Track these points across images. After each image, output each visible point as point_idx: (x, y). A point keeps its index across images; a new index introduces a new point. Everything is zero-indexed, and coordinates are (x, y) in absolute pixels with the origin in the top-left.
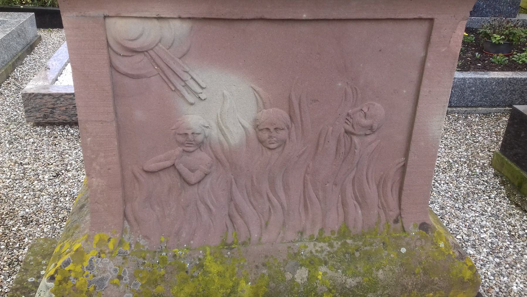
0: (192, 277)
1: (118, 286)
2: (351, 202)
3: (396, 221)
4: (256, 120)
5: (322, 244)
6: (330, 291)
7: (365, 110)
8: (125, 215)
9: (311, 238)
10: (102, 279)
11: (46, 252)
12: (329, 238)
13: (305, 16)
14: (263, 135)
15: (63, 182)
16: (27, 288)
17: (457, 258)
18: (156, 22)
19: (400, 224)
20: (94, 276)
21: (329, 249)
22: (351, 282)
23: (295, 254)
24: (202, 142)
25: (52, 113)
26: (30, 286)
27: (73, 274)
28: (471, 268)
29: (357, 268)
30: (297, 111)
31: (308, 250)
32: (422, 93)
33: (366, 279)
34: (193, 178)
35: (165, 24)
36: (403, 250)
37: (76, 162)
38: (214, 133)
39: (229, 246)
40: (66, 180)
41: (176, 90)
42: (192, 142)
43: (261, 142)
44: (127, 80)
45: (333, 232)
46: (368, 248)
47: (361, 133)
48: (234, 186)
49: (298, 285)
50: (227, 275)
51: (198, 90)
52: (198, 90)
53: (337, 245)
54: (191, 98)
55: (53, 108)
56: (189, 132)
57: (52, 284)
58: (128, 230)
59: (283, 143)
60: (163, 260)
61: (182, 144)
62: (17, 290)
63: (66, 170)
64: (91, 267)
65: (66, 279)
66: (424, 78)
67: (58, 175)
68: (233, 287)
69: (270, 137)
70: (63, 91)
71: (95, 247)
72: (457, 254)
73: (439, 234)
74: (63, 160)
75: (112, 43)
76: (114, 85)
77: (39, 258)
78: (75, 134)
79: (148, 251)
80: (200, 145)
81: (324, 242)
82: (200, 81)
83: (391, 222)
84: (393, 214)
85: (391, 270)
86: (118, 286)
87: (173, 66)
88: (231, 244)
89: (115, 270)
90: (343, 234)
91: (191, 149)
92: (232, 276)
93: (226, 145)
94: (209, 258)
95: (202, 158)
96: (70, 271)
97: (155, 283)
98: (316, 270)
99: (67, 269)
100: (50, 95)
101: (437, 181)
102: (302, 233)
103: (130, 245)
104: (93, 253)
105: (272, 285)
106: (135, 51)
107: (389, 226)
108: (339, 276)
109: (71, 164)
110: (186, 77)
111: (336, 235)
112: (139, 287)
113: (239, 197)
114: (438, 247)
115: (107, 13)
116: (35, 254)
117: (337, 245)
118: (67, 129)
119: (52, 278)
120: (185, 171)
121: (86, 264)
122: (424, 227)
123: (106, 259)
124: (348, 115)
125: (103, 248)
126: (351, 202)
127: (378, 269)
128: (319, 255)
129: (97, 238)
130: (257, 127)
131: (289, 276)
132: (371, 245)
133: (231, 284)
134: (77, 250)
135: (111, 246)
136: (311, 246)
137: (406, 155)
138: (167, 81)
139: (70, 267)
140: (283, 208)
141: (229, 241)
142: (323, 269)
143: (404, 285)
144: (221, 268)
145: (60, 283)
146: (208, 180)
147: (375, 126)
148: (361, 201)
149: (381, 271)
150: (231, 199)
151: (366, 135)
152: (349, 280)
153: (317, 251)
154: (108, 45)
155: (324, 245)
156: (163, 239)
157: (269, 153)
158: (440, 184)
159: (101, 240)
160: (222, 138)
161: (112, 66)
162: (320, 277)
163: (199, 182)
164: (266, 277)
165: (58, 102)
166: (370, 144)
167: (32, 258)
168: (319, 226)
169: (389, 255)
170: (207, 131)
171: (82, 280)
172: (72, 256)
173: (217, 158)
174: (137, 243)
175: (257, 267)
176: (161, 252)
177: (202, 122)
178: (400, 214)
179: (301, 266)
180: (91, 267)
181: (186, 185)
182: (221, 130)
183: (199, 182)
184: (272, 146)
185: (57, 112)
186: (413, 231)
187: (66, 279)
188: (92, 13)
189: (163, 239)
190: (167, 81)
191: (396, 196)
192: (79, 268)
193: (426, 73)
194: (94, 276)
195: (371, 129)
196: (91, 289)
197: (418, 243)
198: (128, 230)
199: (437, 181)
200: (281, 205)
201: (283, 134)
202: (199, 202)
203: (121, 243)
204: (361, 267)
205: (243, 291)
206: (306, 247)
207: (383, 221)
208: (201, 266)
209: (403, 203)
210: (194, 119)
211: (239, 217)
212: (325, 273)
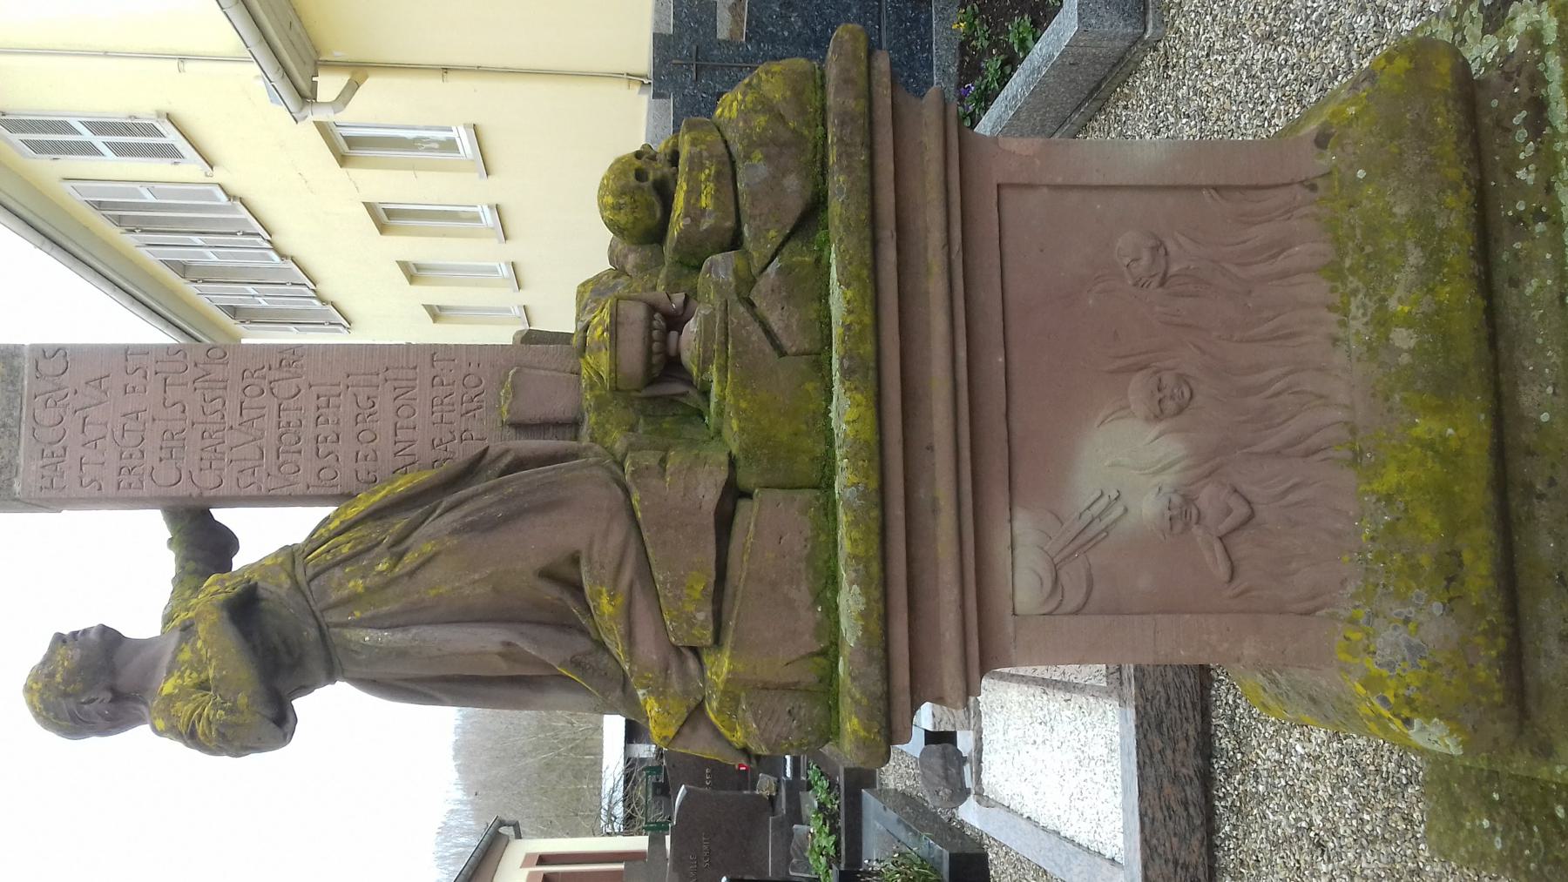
0: (1406, 510)
1: (1421, 624)
2: (1280, 264)
3: (1313, 188)
4: (1147, 419)
5: (1353, 308)
6: (1431, 291)
7: (1127, 261)
8: (1308, 613)
9: (1343, 324)
10: (1410, 648)
11: (1452, 824)
12: (1342, 295)
13: (1001, 359)
14: (1169, 407)
15: (1334, 832)
16: (1512, 849)
17: (1373, 84)
18: (1017, 552)
19: (1320, 183)
20: (1404, 660)
21: (1361, 296)
22: (1415, 257)
23: (1369, 349)
24: (1184, 496)
25: (1185, 867)
26: (1509, 843)
27: (1401, 692)
28: (1389, 58)
29: (1391, 249)
30: (1131, 360)
31: (1360, 327)
32: (1100, 182)
33: (1409, 234)
34: (1241, 511)
35: (1019, 540)
36: (1361, 174)
37: (1291, 809)
38: (1168, 478)
39: (1357, 455)
40: (1328, 825)
41: (1106, 530)
42: (1183, 512)
43: (1180, 410)
44: (1096, 594)
45: (1333, 290)
46: (1358, 232)
47: (1163, 262)
48: (1255, 449)
49: (1419, 344)
50: (1404, 456)
51: (1105, 500)
52: (1105, 500)
53: (1353, 282)
54: (1117, 511)
55: (1176, 863)
56: (1168, 514)
57: (1417, 722)
58: (1331, 610)
59: (1182, 379)
60: (1380, 557)
61: (1187, 527)
62: (1515, 867)
63: (1309, 829)
64: (1390, 665)
65: (1409, 702)
66: (1078, 183)
67: (1319, 845)
68: (1422, 447)
69: (1172, 397)
70: (1137, 837)
71: (1357, 661)
72: (1366, 84)
73: (1334, 115)
74: (1287, 839)
75: (1047, 609)
76: (1102, 612)
77: (1463, 835)
78: (1233, 821)
79: (1365, 580)
80: (1188, 500)
81: (1349, 303)
82: (1092, 499)
83: (1316, 196)
84: (1301, 194)
85: (1394, 194)
86: (1421, 624)
87: (1074, 532)
88: (1354, 451)
89: (1395, 628)
90: (1335, 272)
91: (1194, 512)
92: (1405, 450)
93: (1183, 464)
94: (1376, 486)
95: (1207, 496)
96: (1396, 696)
97: (1414, 571)
98: (1394, 315)
99: (1392, 700)
100: (1145, 867)
101: (1308, 17)
102: (1335, 341)
103: (1356, 607)
104: (1370, 664)
105: (1419, 385)
106: (1056, 580)
107: (1322, 199)
108: (1404, 277)
109: (1297, 820)
110: (1087, 517)
111: (1339, 284)
112: (1423, 593)
113: (1274, 441)
114: (1356, 116)
115: (1010, 611)
116: (1455, 844)
117: (1353, 282)
118: (1223, 840)
119: (1407, 722)
120: (1229, 522)
121: (1385, 672)
122: (1322, 140)
123: (1379, 643)
124: (1135, 285)
125: (1360, 647)
126: (1280, 264)
127: (1394, 215)
128: (1370, 311)
129: (1343, 657)
130: (1158, 418)
131: (1405, 359)
132: (1353, 227)
133: (1418, 450)
134: (1364, 686)
135: (1356, 636)
136: (1356, 325)
137: (1199, 188)
138: (1094, 541)
139: (1390, 695)
140: (1291, 372)
141: (1349, 455)
142: (1393, 304)
143: (1421, 171)
144: (1392, 467)
145: (1415, 710)
146: (1244, 488)
147: (1151, 243)
148: (1279, 247)
149: (1395, 210)
150: (1277, 453)
151: (1166, 253)
152: (1412, 260)
153: (1364, 315)
154: (1050, 614)
155: (1354, 303)
156: (1346, 558)
157: (1198, 398)
158: (1315, 10)
159: (1348, 651)
160: (1177, 467)
161: (1076, 612)
162: (1406, 309)
163: (1249, 503)
164: (1406, 394)
165: (1160, 850)
166: (1180, 246)
167: (1462, 851)
168: (1324, 313)
169: (1368, 197)
170: (1166, 489)
171: (1410, 678)
172: (1373, 693)
173: (1210, 475)
174: (1354, 597)
175: (1390, 410)
176: (1366, 561)
177: (1151, 496)
178: (1301, 182)
179: (1388, 339)
180: (1390, 665)
181: (1254, 521)
182: (1164, 469)
183: (1249, 503)
184: (1187, 394)
185: (1183, 856)
186: (1330, 158)
187: (1409, 702)
188: (1010, 629)
189: (1346, 558)
190: (1094, 541)
191: (1269, 193)
192: (1392, 683)
193: (1071, 181)
194: (1404, 660)
195: (1158, 247)
196: (1424, 663)
197: (1350, 149)
198: (1331, 610)
199: (1308, 17)
200: (1285, 375)
201: (1168, 379)
202: (1283, 502)
203: (1353, 621)
204: (1389, 242)
205: (1430, 431)
206: (1358, 332)
207: (1314, 209)
208: (1389, 499)
209: (1280, 181)
210: (1148, 507)
211: (1309, 441)
212: (1400, 300)
